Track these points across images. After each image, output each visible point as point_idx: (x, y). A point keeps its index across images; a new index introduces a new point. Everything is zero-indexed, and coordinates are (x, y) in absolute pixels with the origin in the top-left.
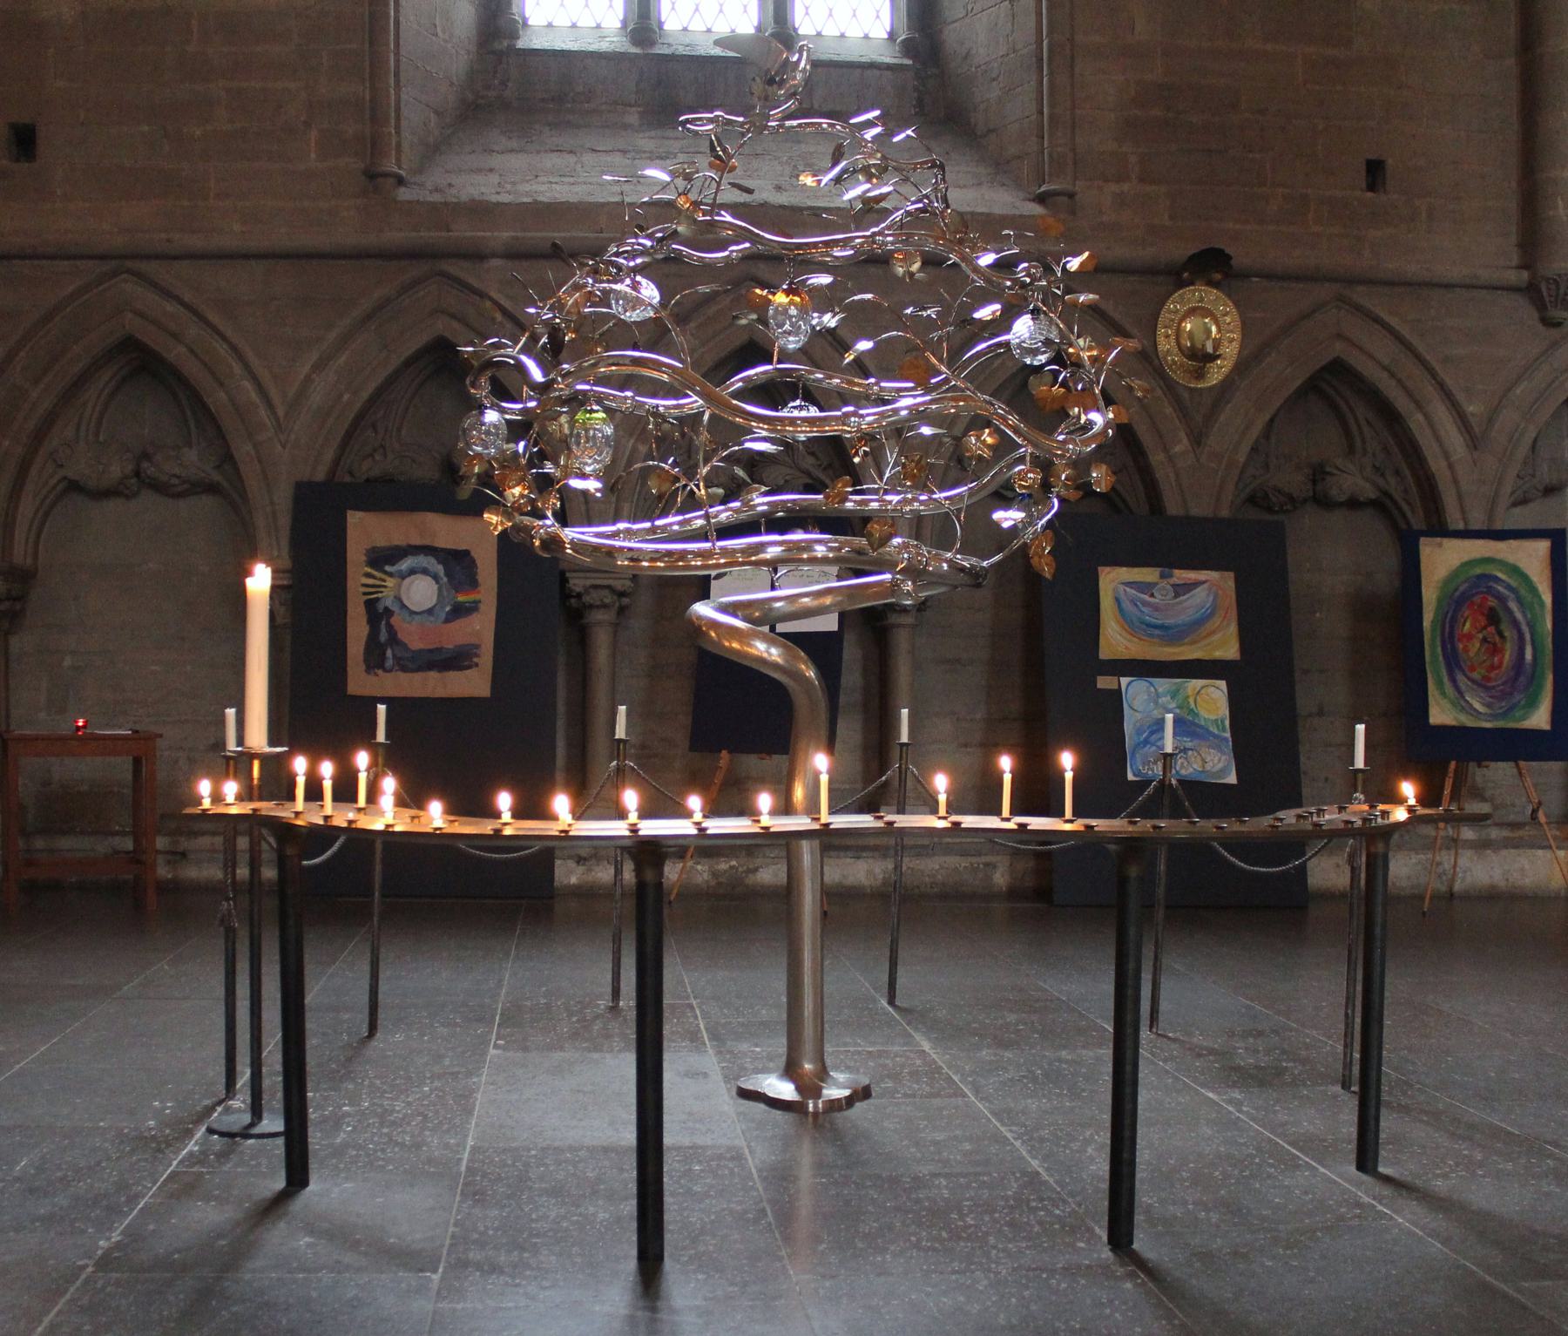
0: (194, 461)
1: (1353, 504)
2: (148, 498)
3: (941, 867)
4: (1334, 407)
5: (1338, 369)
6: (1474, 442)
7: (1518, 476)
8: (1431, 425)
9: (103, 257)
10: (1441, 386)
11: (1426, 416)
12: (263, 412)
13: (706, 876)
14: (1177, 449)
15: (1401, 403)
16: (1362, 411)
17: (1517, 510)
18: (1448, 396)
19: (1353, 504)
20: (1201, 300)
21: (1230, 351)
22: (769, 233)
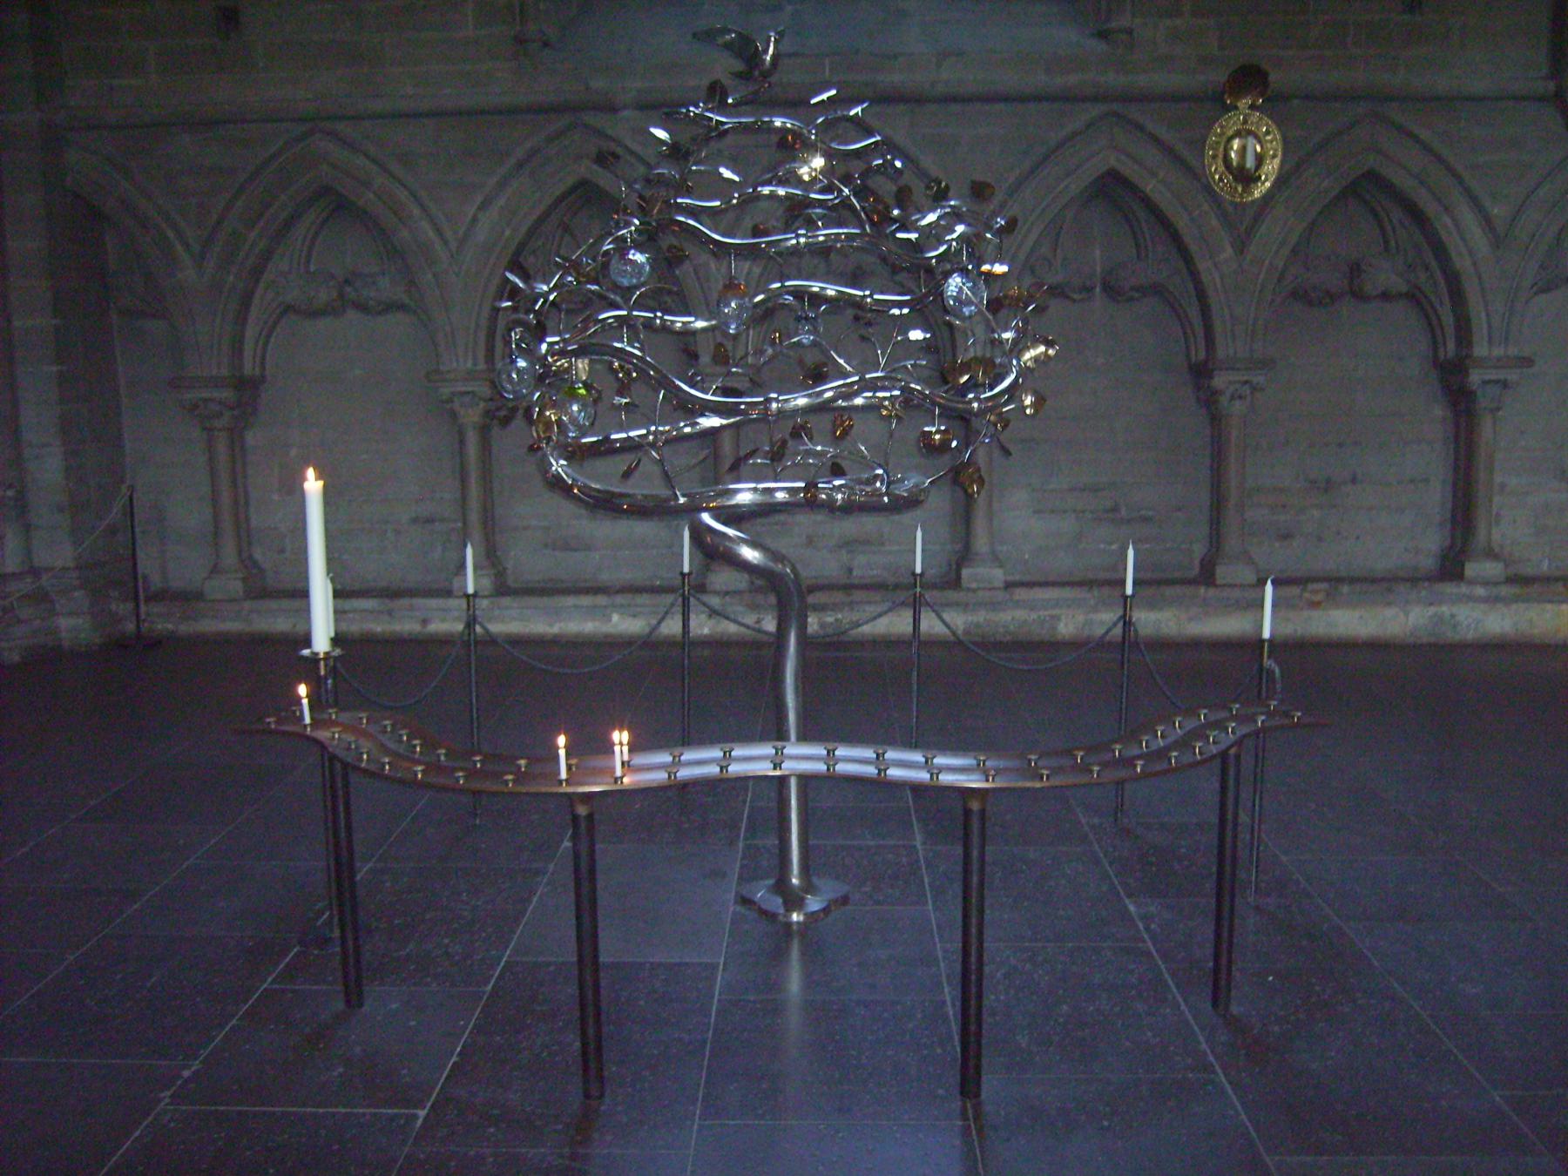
0: (387, 287)
1: (1385, 296)
2: (352, 314)
3: (1013, 619)
4: (1373, 212)
5: (1373, 177)
6: (1498, 241)
7: (1541, 266)
8: (1457, 226)
9: (301, 120)
10: (1467, 191)
11: (1454, 220)
12: (439, 247)
13: (816, 627)
14: (1223, 256)
15: (1430, 207)
16: (1397, 214)
17: (1542, 299)
18: (1474, 201)
19: (1385, 296)
20: (1245, 122)
21: (1271, 168)
22: (855, 143)
